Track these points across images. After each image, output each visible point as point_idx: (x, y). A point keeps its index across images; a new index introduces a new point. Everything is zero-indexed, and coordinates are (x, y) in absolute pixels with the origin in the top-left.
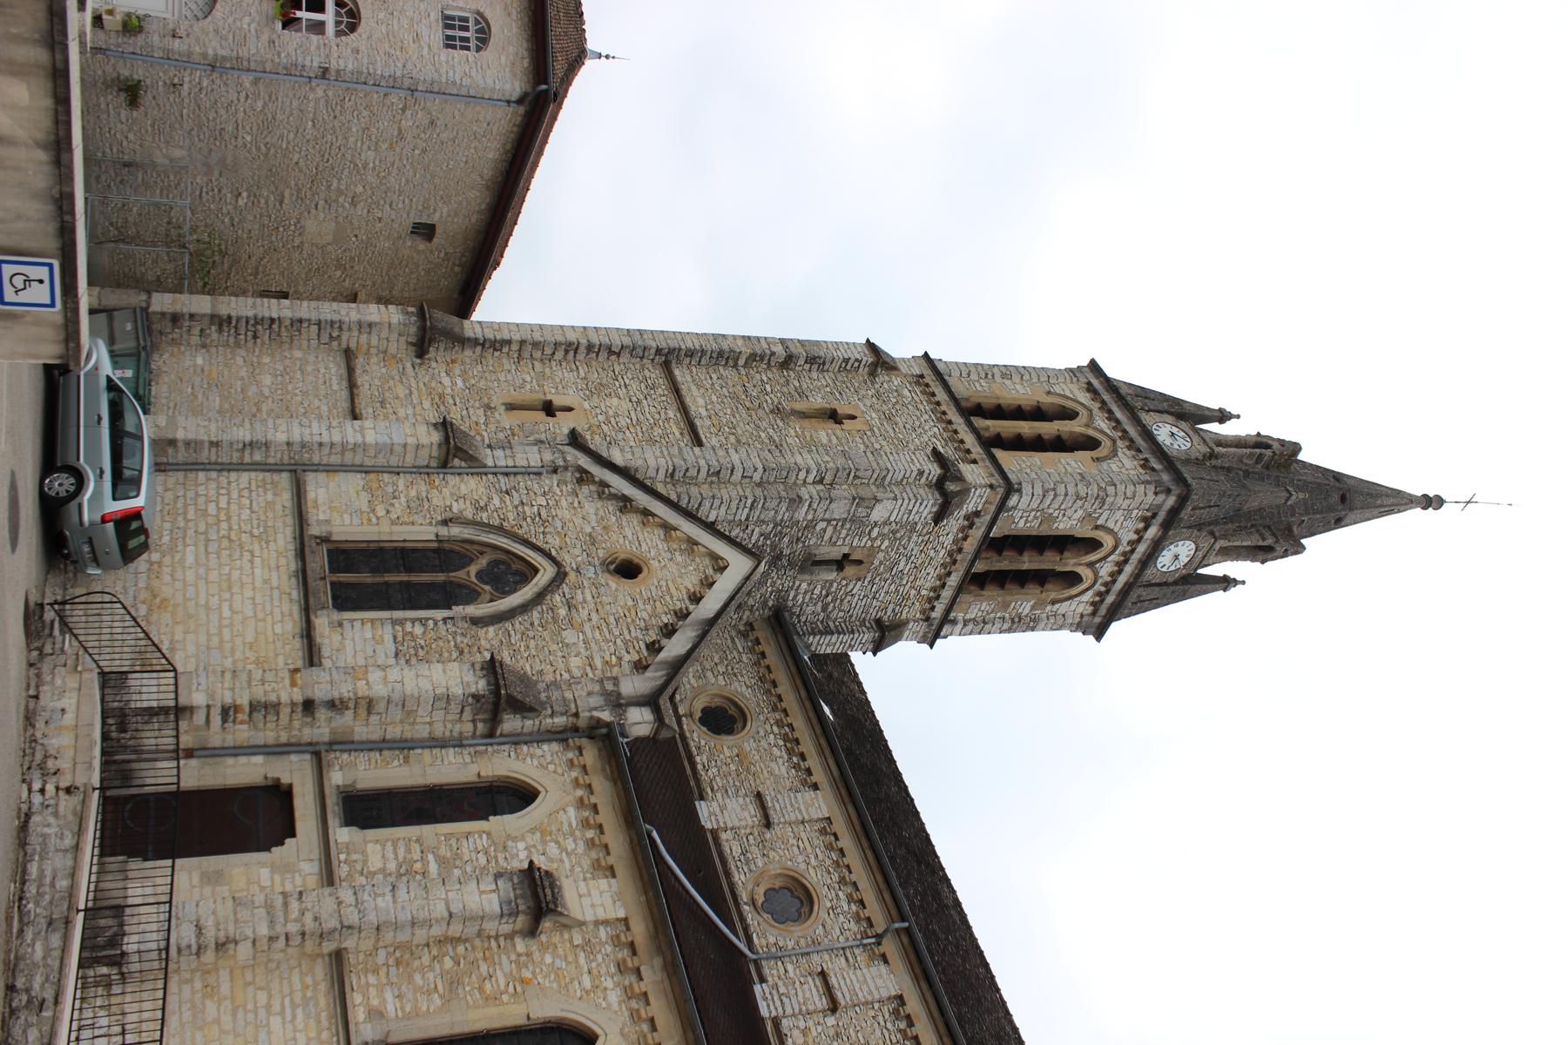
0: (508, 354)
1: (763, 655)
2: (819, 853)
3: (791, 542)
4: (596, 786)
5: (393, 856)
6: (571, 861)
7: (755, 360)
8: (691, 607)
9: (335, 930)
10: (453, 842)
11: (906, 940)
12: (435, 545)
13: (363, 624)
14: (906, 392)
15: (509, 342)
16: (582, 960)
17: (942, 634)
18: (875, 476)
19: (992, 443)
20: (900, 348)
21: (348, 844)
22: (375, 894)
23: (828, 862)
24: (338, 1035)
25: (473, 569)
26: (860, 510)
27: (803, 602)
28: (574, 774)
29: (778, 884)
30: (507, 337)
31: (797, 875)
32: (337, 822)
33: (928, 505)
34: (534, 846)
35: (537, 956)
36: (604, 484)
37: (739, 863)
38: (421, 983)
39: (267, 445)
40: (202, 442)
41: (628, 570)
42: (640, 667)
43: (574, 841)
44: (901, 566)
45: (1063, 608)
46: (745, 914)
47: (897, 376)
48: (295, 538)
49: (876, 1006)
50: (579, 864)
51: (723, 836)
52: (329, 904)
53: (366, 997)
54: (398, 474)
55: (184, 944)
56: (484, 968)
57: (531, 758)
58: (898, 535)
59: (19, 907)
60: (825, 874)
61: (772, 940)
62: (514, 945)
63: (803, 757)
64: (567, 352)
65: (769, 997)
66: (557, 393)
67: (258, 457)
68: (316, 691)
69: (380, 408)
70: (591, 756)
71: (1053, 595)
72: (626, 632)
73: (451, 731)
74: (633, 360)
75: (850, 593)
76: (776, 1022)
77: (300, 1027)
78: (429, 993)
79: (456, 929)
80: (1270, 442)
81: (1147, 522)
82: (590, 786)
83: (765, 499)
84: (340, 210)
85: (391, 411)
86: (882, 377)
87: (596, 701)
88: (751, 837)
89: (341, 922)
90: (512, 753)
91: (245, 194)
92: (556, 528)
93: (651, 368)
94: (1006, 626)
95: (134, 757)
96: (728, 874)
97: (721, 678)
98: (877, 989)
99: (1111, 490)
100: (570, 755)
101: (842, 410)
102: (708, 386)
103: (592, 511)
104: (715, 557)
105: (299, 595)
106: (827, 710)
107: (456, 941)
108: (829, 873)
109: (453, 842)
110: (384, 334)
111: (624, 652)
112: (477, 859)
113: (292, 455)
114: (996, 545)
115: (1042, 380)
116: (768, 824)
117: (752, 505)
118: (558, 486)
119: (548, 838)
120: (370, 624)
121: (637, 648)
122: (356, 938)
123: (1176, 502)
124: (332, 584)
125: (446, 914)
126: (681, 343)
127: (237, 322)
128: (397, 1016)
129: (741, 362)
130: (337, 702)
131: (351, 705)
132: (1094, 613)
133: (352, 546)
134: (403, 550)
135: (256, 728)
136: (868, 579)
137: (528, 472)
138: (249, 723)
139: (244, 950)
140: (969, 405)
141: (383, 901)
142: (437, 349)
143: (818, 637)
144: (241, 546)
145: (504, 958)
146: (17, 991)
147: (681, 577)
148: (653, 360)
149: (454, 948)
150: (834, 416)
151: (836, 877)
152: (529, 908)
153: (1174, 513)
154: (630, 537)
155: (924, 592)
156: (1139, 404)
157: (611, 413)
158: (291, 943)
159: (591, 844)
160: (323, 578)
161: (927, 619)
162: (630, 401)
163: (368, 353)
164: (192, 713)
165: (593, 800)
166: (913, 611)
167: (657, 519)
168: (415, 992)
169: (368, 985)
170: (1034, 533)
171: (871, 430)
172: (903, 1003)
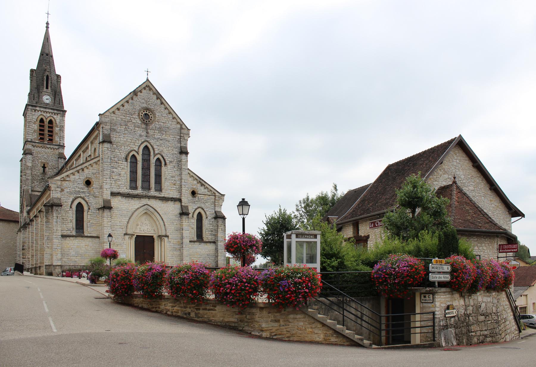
45: (58, 121)
161: (58, 148)
166: (57, 152)
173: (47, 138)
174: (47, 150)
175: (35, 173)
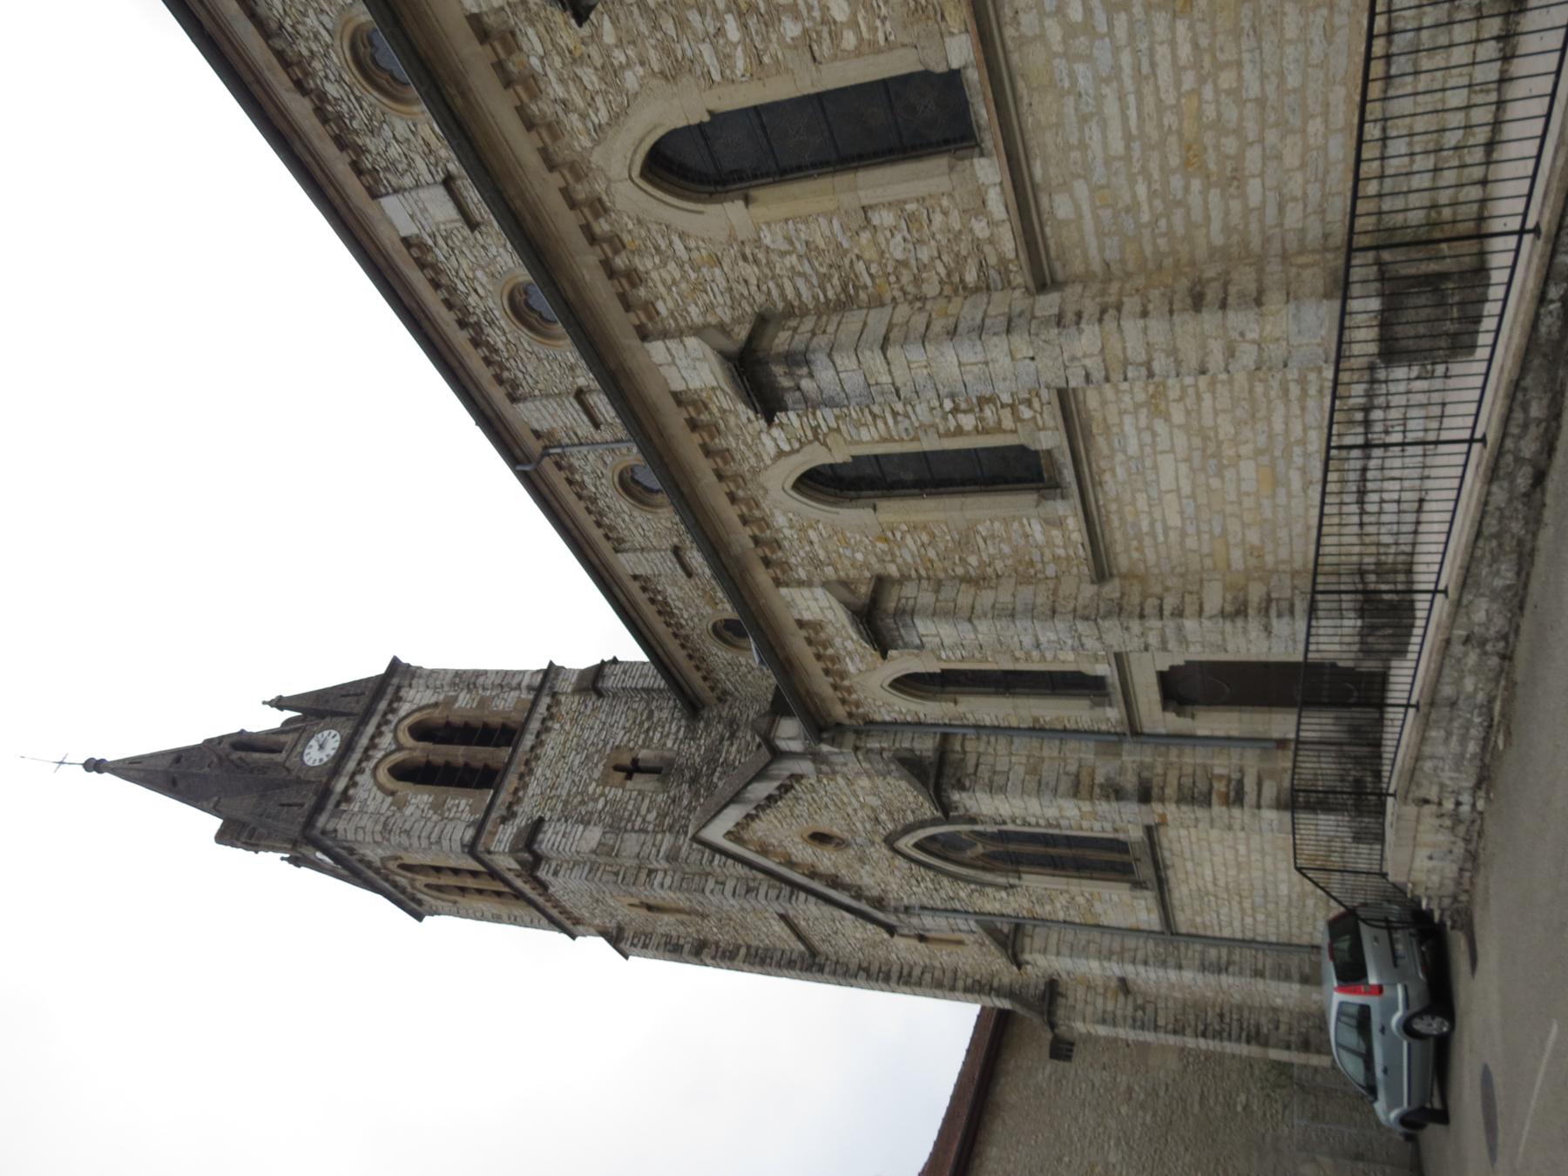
1: (705, 679)
3: (681, 798)
7: (731, 952)
9: (1104, 618)
11: (518, 452)
17: (541, 676)
18: (599, 874)
23: (611, 515)
26: (611, 842)
27: (671, 723)
32: (1110, 681)
33: (548, 840)
38: (1002, 546)
39: (1203, 968)
40: (1272, 977)
42: (797, 778)
45: (428, 697)
49: (537, 392)
55: (1286, 619)
56: (931, 553)
58: (579, 798)
59: (1492, 720)
62: (899, 570)
64: (910, 975)
67: (1213, 952)
73: (989, 742)
75: (628, 730)
77: (1143, 516)
79: (965, 597)
81: (345, 797)
84: (1143, 1083)
86: (611, 925)
89: (1097, 624)
91: (1239, 1108)
94: (481, 680)
95: (1346, 748)
97: (744, 662)
99: (378, 838)
101: (644, 912)
107: (966, 579)
110: (1090, 1009)
114: (487, 778)
122: (1080, 599)
123: (316, 821)
125: (976, 622)
127: (1240, 1036)
128: (1028, 520)
129: (743, 951)
130: (1112, 796)
131: (1097, 790)
132: (399, 688)
135: (1205, 767)
136: (609, 747)
138: (1213, 775)
139: (1213, 601)
142: (1036, 988)
143: (656, 686)
144: (1227, 889)
146: (1498, 654)
148: (827, 959)
151: (601, 503)
152: (882, 620)
153: (318, 808)
155: (557, 726)
158: (1156, 602)
161: (554, 695)
163: (1106, 989)
164: (1278, 799)
166: (569, 703)
168: (1009, 538)
169: (1065, 547)
170: (452, 790)
173: (481, 755)
174: (549, 750)
175: (651, 817)
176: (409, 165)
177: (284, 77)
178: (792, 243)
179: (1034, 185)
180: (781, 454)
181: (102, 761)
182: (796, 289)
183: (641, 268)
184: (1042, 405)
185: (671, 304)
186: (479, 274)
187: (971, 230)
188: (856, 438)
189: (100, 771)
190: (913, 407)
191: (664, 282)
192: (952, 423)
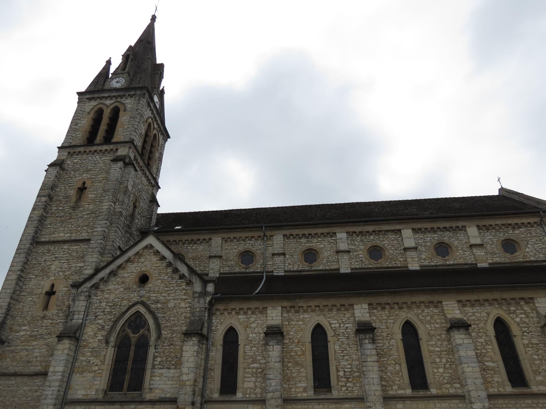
0: (14, 305)
2: (233, 244)
4: (233, 307)
5: (250, 378)
6: (259, 320)
7: (46, 209)
8: (167, 261)
10: (246, 357)
11: (268, 228)
12: (116, 348)
13: (152, 380)
14: (76, 161)
15: (10, 303)
16: (294, 323)
18: (118, 184)
19: (108, 139)
20: (53, 156)
21: (243, 394)
22: (270, 386)
24: (310, 403)
25: (132, 335)
28: (226, 313)
29: (240, 259)
30: (7, 304)
31: (239, 253)
32: (234, 397)
34: (252, 331)
35: (290, 337)
36: (102, 279)
37: (232, 269)
41: (144, 279)
43: (251, 318)
44: (140, 187)
46: (249, 271)
47: (66, 161)
48: (103, 405)
49: (285, 242)
50: (260, 318)
51: (222, 271)
52: (272, 402)
53: (299, 392)
54: (77, 359)
56: (293, 354)
57: (217, 326)
60: (241, 245)
61: (259, 266)
63: (199, 240)
64: (21, 281)
65: (278, 271)
66: (42, 289)
68: (188, 400)
69: (32, 364)
70: (221, 307)
71: (157, 145)
72: (172, 285)
74: (32, 255)
76: (285, 271)
78: (299, 372)
80: (127, 54)
82: (232, 309)
83: (118, 224)
85: (34, 359)
87: (202, 301)
88: (224, 263)
89: (279, 398)
90: (214, 333)
92: (119, 301)
93: (38, 249)
96: (236, 273)
98: (280, 241)
99: (139, 111)
100: (218, 313)
101: (80, 185)
102: (54, 230)
103: (113, 286)
104: (146, 247)
105: (133, 405)
106: (177, 228)
108: (240, 243)
109: (246, 357)
111: (181, 288)
112: (254, 350)
113: (58, 404)
115: (81, 113)
116: (220, 257)
117: (118, 229)
118: (97, 297)
119: (249, 326)
120: (153, 378)
121: (180, 283)
124: (128, 391)
126: (31, 234)
128: (306, 383)
129: (45, 214)
133: (110, 382)
134: (116, 361)
137: (87, 308)
140: (102, 141)
141: (273, 383)
142: (3, 335)
145: (290, 347)
147: (151, 261)
148: (34, 248)
149: (285, 362)
150: (82, 189)
151: (242, 242)
154: (129, 275)
156: (100, 87)
157: (59, 270)
159: (253, 313)
160: (126, 394)
162: (54, 261)
165: (238, 309)
167: (124, 264)
168: (299, 376)
171: (92, 178)
172: (305, 234)
176: (353, 244)
177: (377, 229)
178: (392, 346)
179: (405, 400)
180: (331, 324)
181: (155, 21)
182: (380, 343)
183: (386, 310)
184: (346, 393)
185: (376, 313)
186: (322, 246)
187: (395, 385)
188: (336, 344)
189: (151, 20)
190: (346, 361)
191: (383, 314)
192: (340, 370)
